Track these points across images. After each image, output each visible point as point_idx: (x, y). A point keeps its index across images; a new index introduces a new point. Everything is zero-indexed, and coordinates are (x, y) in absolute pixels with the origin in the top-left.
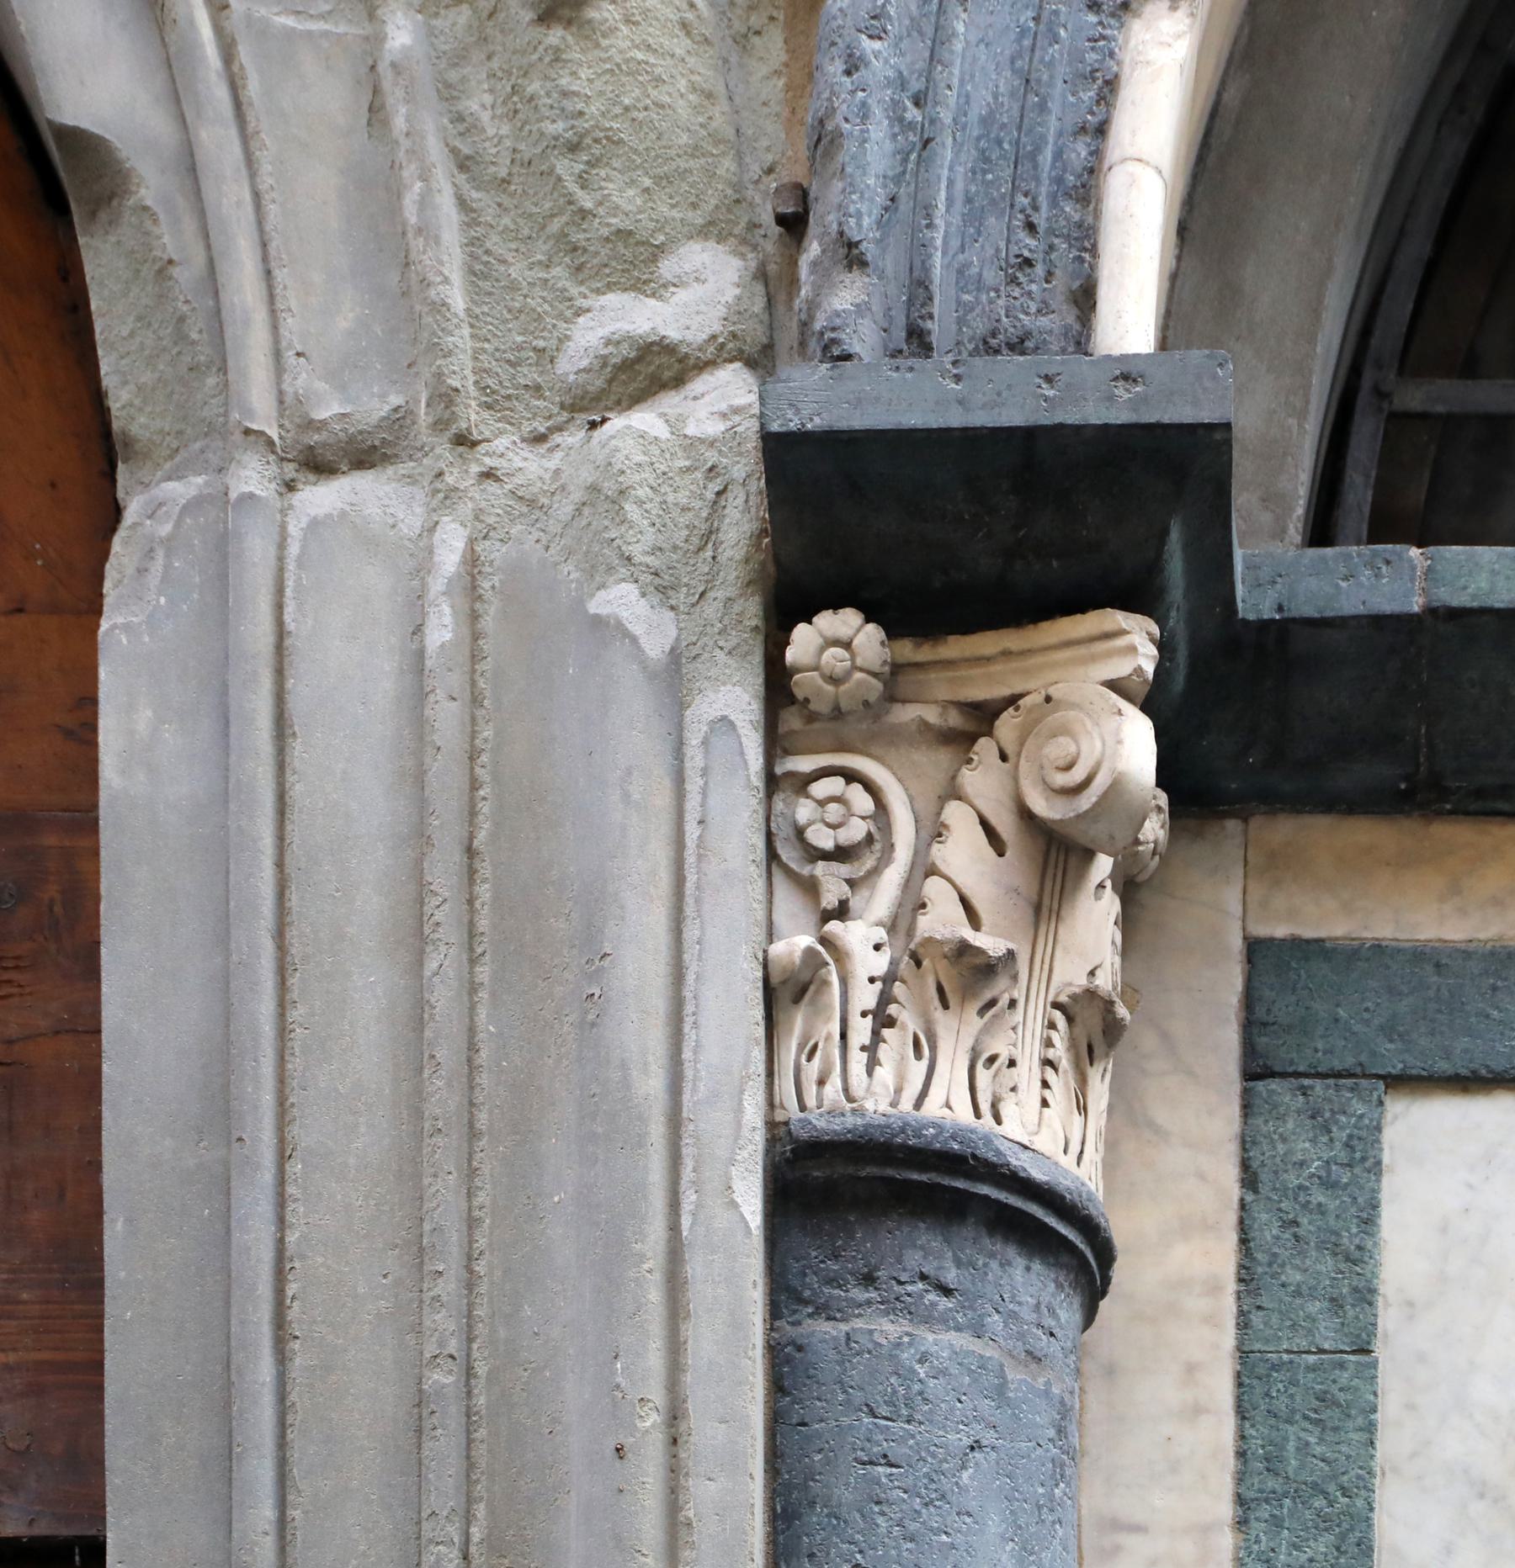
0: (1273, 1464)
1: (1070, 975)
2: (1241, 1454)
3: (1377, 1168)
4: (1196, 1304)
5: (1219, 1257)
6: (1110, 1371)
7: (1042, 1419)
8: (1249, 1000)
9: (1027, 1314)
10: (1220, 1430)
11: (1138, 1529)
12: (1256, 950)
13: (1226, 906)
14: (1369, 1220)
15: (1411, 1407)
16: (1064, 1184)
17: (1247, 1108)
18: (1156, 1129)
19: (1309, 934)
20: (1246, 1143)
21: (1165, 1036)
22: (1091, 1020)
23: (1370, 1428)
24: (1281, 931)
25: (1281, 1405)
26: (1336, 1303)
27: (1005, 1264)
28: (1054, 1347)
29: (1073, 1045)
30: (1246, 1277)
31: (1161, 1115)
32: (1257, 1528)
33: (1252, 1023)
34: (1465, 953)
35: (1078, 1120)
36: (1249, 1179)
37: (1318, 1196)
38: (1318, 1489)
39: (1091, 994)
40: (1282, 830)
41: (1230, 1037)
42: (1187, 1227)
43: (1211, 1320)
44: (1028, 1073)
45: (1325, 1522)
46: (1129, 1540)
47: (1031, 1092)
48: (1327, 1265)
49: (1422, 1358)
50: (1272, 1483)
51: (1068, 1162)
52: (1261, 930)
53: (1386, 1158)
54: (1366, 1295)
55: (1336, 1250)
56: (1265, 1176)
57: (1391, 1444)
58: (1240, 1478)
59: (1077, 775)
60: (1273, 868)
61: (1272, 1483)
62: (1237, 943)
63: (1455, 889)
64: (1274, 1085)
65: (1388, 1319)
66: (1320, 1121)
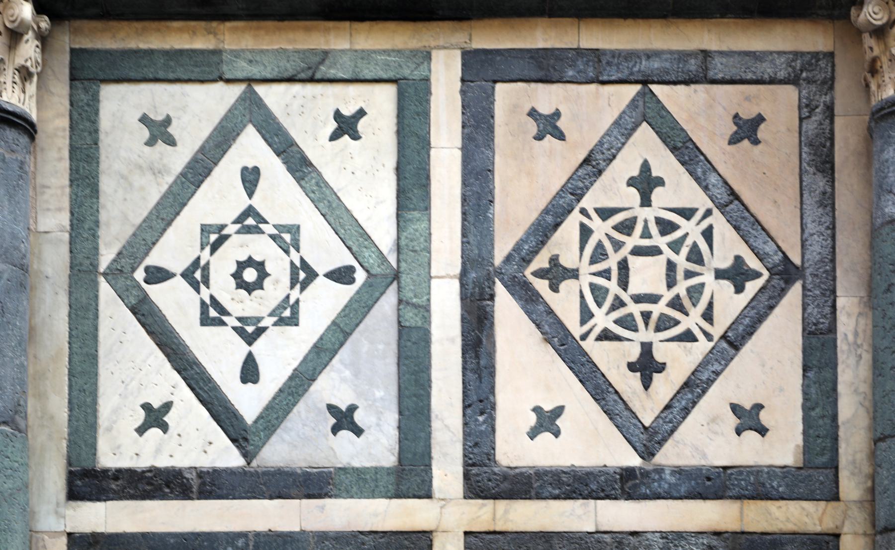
0: (77, 171)
1: (19, 61)
2: (71, 169)
3: (98, 101)
4: (60, 134)
5: (65, 122)
6: (42, 150)
7: (15, 166)
8: (71, 62)
9: (11, 141)
10: (66, 164)
11: (49, 187)
12: (73, 51)
13: (65, 41)
14: (97, 112)
15: (107, 157)
16: (17, 110)
17: (71, 88)
18: (53, 94)
19: (83, 47)
20: (71, 96)
21: (53, 71)
22: (24, 71)
23: (98, 163)
24: (77, 46)
25: (79, 157)
26: (90, 133)
27: (4, 130)
28: (19, 148)
29: (21, 78)
30: (72, 127)
31: (53, 90)
32: (74, 186)
33: (72, 68)
34: (116, 51)
35: (22, 95)
36: (72, 104)
37: (86, 108)
38: (87, 177)
39: (23, 66)
40: (77, 23)
41: (67, 71)
42: (59, 115)
43: (64, 137)
44: (9, 85)
45: (89, 185)
46: (47, 190)
47: (10, 89)
48: (88, 124)
49: (109, 145)
50: (77, 176)
51: (20, 105)
52: (73, 46)
53: (101, 98)
54: (97, 131)
55: (90, 121)
56: (75, 104)
57: (103, 166)
58: (71, 175)
59: (14, 18)
60: (75, 32)
61: (77, 176)
62: (68, 49)
63: (114, 36)
64: (77, 82)
65: (102, 136)
66: (86, 90)
